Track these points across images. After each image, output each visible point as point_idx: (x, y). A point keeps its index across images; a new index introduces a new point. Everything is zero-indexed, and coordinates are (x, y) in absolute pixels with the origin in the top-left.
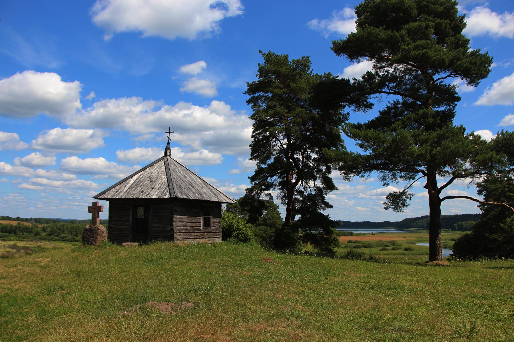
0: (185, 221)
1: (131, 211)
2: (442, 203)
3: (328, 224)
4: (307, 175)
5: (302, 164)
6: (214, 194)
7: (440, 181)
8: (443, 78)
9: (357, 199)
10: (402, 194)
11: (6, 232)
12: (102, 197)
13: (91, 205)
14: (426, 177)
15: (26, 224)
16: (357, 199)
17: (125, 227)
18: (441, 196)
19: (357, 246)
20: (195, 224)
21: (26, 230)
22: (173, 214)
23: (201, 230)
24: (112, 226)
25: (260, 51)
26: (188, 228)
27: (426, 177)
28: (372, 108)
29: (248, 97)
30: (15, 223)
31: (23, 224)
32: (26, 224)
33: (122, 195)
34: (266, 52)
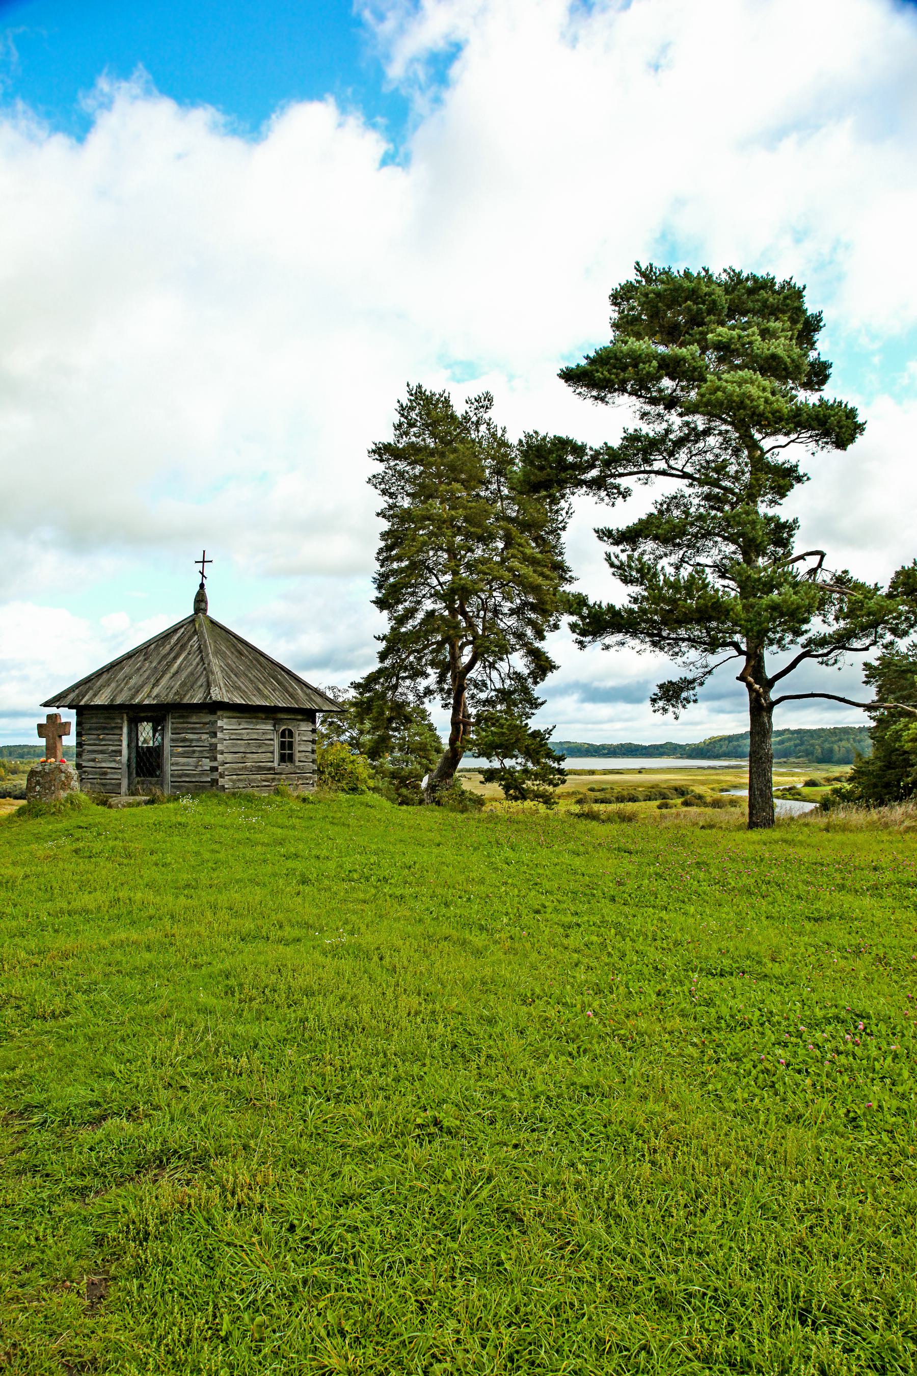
2: (776, 710)
3: (537, 746)
4: (491, 648)
5: (484, 622)
6: (169, 654)
7: (774, 660)
13: (44, 721)
14: (744, 657)
17: (113, 765)
23: (273, 769)
24: (84, 764)
27: (744, 657)
33: (101, 700)
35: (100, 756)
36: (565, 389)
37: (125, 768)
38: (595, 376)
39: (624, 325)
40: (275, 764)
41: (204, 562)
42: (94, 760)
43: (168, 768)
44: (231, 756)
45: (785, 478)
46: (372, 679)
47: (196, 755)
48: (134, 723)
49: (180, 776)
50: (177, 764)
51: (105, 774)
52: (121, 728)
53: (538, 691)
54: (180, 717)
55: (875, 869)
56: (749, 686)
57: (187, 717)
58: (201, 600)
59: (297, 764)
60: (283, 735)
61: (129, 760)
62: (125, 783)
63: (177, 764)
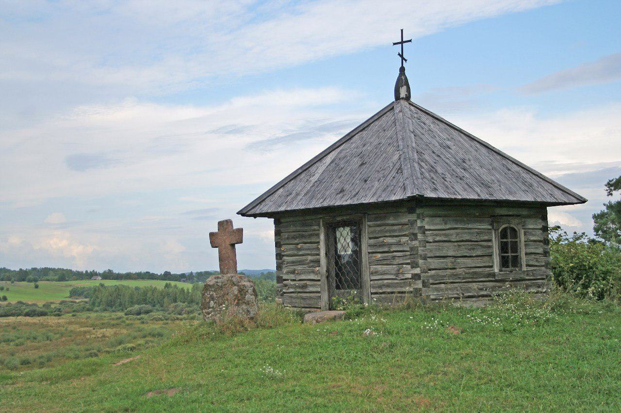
0: (451, 253)
1: (322, 237)
11: (145, 301)
12: (257, 210)
13: (216, 230)
17: (312, 277)
22: (234, 231)
23: (494, 275)
24: (285, 277)
30: (160, 285)
31: (175, 286)
32: (181, 285)
35: (299, 268)
37: (324, 279)
40: (496, 269)
41: (402, 42)
42: (293, 272)
43: (366, 277)
44: (436, 261)
47: (398, 261)
48: (332, 229)
49: (380, 287)
50: (376, 273)
51: (305, 286)
52: (318, 235)
54: (376, 219)
57: (385, 218)
58: (402, 81)
59: (524, 268)
60: (504, 234)
61: (328, 271)
62: (325, 297)
63: (376, 273)
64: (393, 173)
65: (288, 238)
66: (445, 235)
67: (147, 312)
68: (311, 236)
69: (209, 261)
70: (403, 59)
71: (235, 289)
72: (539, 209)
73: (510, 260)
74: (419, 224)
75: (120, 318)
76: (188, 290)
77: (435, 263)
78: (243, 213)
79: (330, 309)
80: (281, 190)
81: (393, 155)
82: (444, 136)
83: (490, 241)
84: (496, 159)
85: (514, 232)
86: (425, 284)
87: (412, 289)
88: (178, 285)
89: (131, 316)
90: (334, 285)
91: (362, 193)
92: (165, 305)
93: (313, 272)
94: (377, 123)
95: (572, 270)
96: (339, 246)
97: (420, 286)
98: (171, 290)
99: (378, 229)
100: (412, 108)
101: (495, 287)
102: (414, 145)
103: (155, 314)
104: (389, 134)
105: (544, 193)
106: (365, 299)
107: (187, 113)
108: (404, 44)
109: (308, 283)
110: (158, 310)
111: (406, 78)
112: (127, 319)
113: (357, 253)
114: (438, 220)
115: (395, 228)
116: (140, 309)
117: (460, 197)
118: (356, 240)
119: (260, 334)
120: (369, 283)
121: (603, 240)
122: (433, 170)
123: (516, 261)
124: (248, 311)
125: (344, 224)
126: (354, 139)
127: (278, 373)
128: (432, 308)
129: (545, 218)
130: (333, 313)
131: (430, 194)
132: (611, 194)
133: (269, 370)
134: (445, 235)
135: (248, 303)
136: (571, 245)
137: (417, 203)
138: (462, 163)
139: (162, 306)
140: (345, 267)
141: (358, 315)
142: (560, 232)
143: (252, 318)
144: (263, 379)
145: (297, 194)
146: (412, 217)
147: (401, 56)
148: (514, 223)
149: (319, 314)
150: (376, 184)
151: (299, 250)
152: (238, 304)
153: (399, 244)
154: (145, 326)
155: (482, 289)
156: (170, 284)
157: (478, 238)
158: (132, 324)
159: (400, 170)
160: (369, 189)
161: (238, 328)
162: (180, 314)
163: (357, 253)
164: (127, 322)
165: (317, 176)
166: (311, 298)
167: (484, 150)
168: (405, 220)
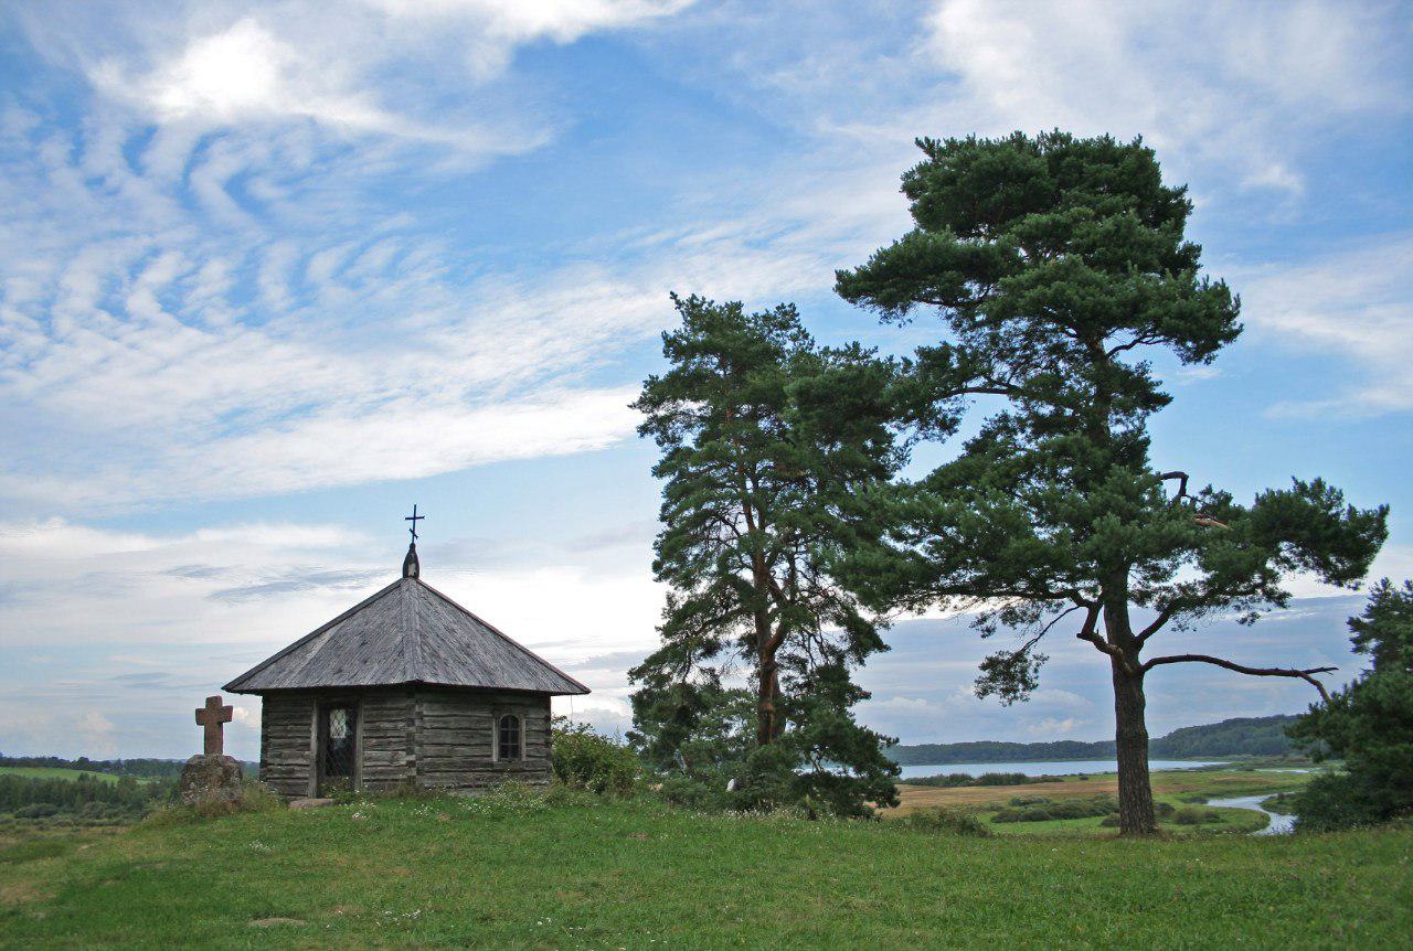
0: (448, 740)
1: (315, 719)
2: (1148, 677)
8: (1127, 348)
9: (924, 671)
10: (1019, 657)
11: (47, 799)
15: (102, 777)
16: (924, 671)
17: (300, 761)
18: (1143, 657)
19: (1034, 814)
20: (477, 751)
21: (112, 797)
23: (492, 765)
24: (270, 761)
25: (672, 293)
26: (455, 759)
28: (956, 431)
29: (641, 418)
30: (72, 777)
32: (102, 777)
33: (290, 682)
34: (684, 296)
35: (286, 751)
36: (1352, 654)
37: (313, 764)
38: (886, 282)
39: (924, 214)
40: (495, 759)
41: (414, 518)
42: (280, 756)
43: (360, 762)
45: (1147, 397)
46: (657, 660)
49: (374, 774)
50: (370, 759)
51: (292, 771)
52: (310, 717)
53: (857, 675)
55: (484, 919)
56: (954, 590)
58: (411, 559)
59: (524, 759)
60: (504, 723)
61: (318, 755)
62: (313, 783)
63: (370, 759)
64: (395, 656)
65: (277, 719)
66: (445, 722)
67: (48, 814)
68: (302, 717)
69: (191, 744)
70: (414, 535)
71: (220, 771)
72: (542, 699)
73: (509, 748)
74: (417, 709)
75: (7, 821)
76: (112, 784)
77: (431, 750)
78: (229, 688)
79: (318, 797)
80: (273, 666)
81: (396, 635)
82: (450, 618)
83: (490, 729)
84: (503, 646)
85: (516, 722)
86: (419, 772)
87: (405, 777)
88: (98, 777)
89: (25, 820)
90: (324, 771)
91: (360, 675)
92: (76, 806)
93: (302, 756)
94: (382, 600)
95: (575, 762)
96: (332, 730)
97: (414, 774)
98: (87, 783)
99: (375, 712)
100: (420, 587)
101: (492, 777)
102: (418, 627)
103: (60, 817)
104: (394, 612)
105: (548, 682)
106: (356, 785)
107: (136, 543)
108: (412, 516)
109: (296, 768)
110: (65, 812)
111: (416, 556)
112: (18, 823)
113: (351, 738)
114: (436, 706)
115: (393, 712)
116: (40, 809)
117: (460, 683)
118: (351, 725)
119: (244, 817)
120: (362, 770)
121: (642, 734)
122: (434, 654)
123: (516, 751)
124: (232, 794)
125: (340, 706)
126: (356, 616)
127: (267, 849)
128: (425, 796)
129: (548, 707)
130: (321, 800)
131: (429, 679)
132: (633, 683)
133: (258, 845)
134: (445, 722)
135: (232, 786)
136: (577, 736)
137: (416, 689)
138: (466, 649)
139: (72, 806)
140: (338, 754)
141: (348, 802)
142: (565, 722)
143: (234, 802)
144: (251, 854)
145: (291, 672)
146: (409, 702)
147: (413, 532)
148: (516, 713)
149: (306, 801)
150: (376, 667)
151: (290, 731)
152: (221, 786)
153: (395, 729)
154: (45, 834)
155: (478, 779)
156: (87, 776)
157: (478, 726)
158: (24, 831)
159: (401, 653)
160: (369, 670)
161: (219, 811)
162: (98, 817)
163: (351, 738)
164: (18, 827)
165: (314, 653)
166: (297, 784)
167: (490, 635)
168: (403, 705)
